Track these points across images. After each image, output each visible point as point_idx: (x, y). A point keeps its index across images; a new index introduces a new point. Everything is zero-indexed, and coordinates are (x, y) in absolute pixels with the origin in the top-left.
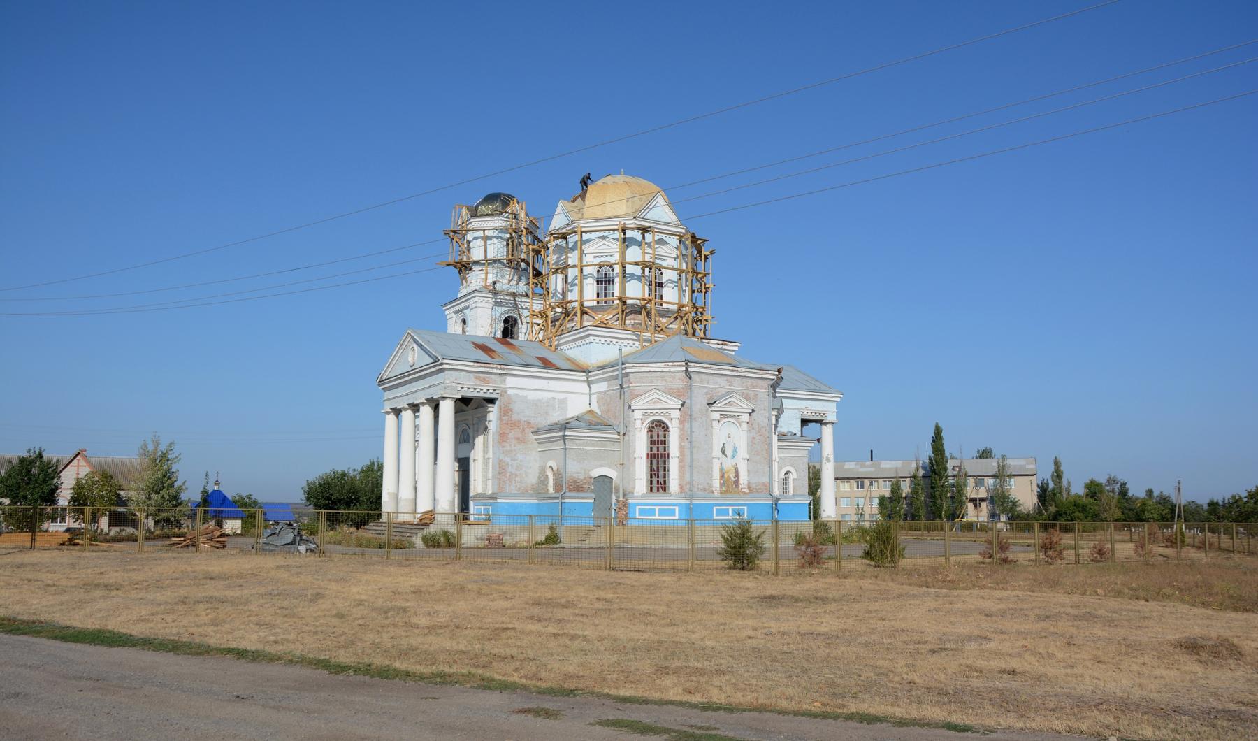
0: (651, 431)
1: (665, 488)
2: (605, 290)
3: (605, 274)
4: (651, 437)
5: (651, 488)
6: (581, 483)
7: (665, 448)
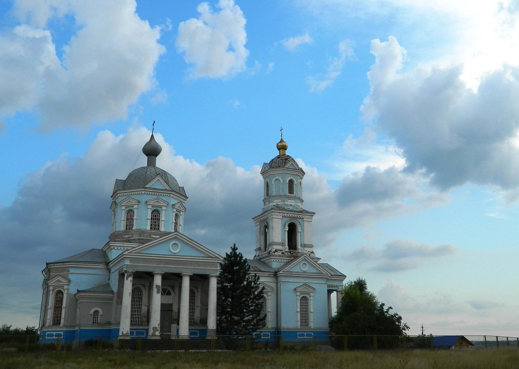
2: (155, 223)
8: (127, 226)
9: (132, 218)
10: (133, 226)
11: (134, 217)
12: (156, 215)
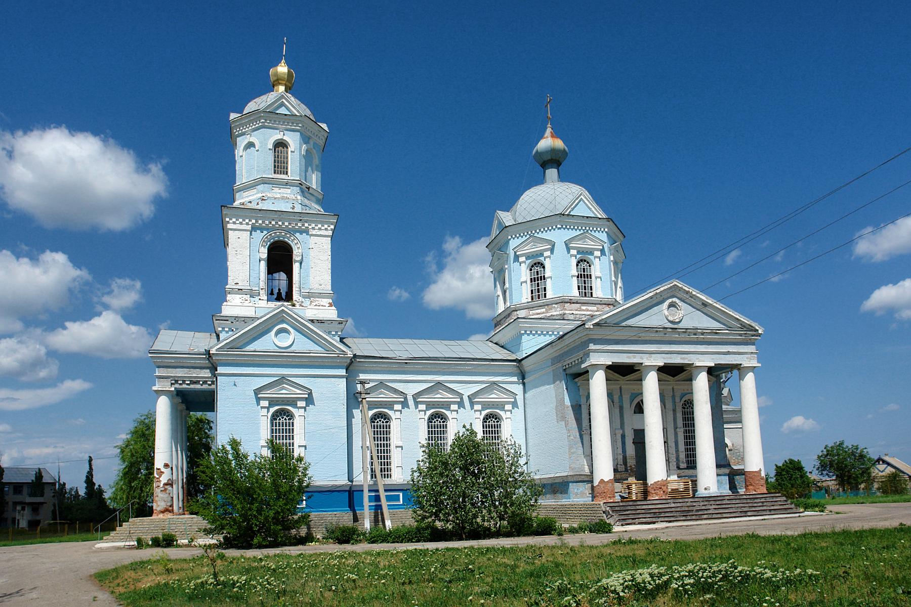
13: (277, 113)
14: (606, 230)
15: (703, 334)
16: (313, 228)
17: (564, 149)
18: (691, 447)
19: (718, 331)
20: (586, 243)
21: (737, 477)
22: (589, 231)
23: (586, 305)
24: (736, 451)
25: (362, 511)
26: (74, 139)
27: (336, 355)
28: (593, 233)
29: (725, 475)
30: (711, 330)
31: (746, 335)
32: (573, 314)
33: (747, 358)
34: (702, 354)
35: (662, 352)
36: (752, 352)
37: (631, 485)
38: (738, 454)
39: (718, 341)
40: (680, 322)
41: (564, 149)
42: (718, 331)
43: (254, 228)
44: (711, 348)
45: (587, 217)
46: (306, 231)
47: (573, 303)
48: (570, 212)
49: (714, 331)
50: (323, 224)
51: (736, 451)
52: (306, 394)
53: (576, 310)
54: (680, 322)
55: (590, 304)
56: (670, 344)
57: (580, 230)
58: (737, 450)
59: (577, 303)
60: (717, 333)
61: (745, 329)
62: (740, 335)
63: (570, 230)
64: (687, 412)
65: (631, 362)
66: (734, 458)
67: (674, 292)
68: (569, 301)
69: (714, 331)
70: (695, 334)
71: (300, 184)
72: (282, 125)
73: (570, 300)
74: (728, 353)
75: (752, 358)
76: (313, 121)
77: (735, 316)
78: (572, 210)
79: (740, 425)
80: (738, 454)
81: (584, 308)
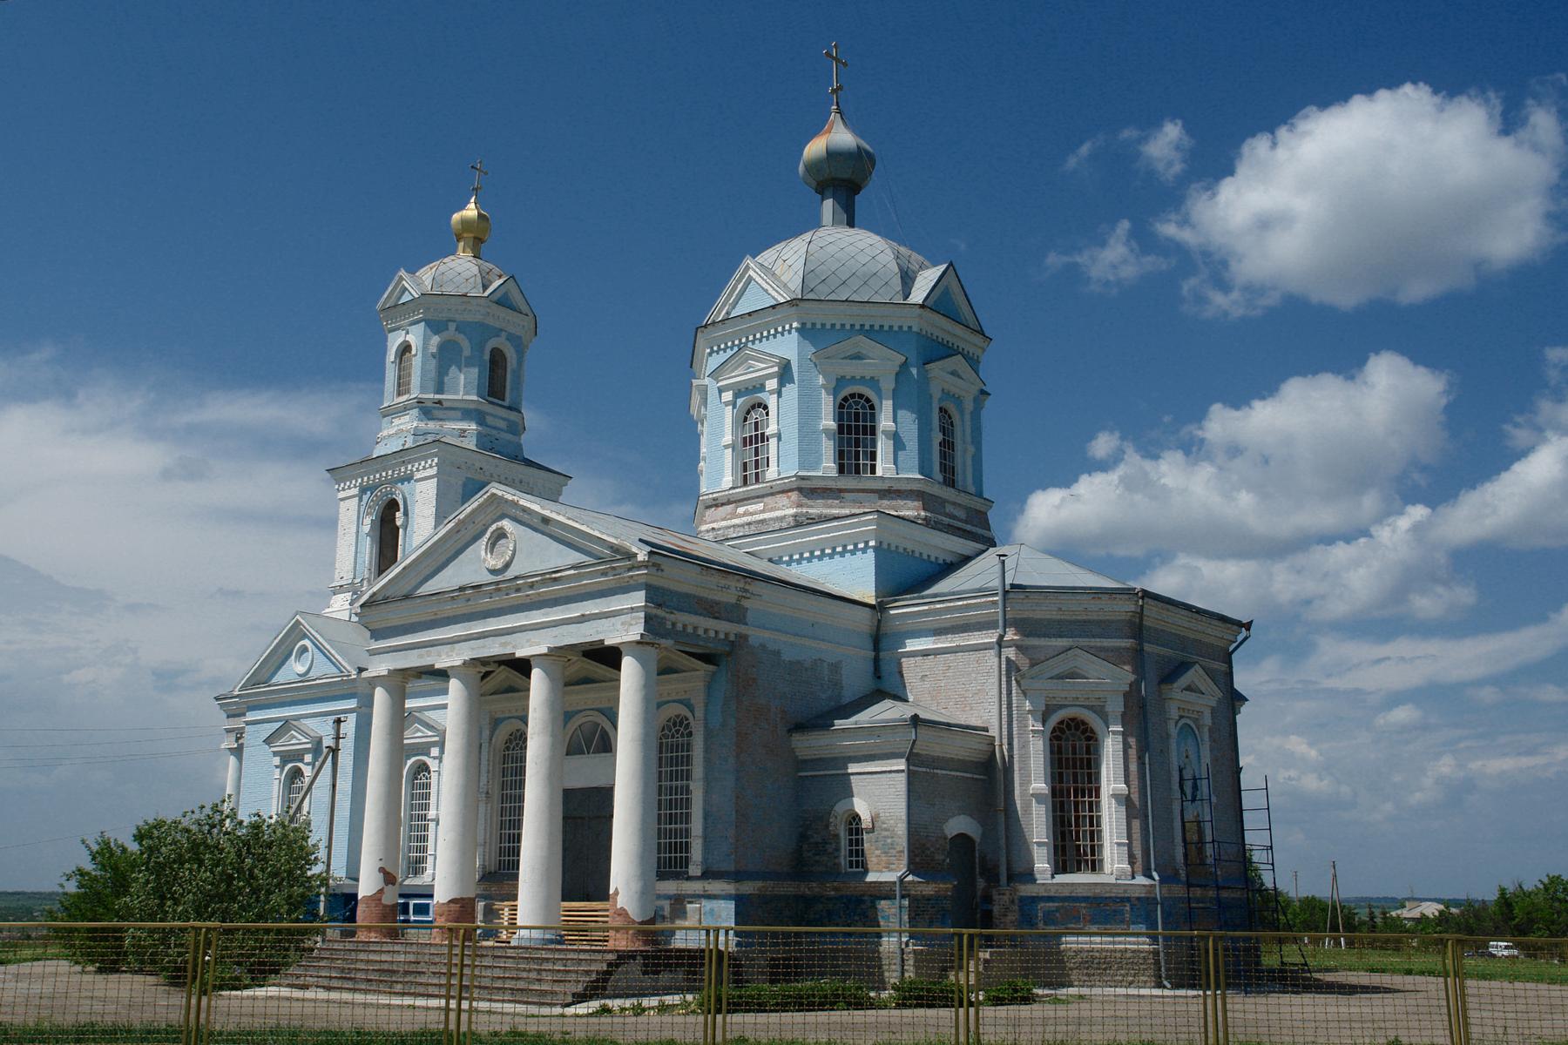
0: (1058, 738)
1: (1093, 862)
3: (857, 414)
4: (1060, 752)
5: (1064, 862)
6: (932, 849)
7: (1090, 775)
8: (745, 470)
9: (763, 434)
10: (768, 466)
11: (768, 426)
12: (857, 414)
13: (403, 304)
14: (795, 325)
15: (532, 586)
16: (418, 470)
17: (858, 147)
18: (422, 844)
19: (554, 576)
20: (752, 369)
21: (883, 902)
22: (750, 345)
23: (745, 502)
24: (886, 833)
25: (514, 921)
26: (1243, 170)
27: (339, 679)
28: (757, 346)
29: (727, 897)
30: (541, 575)
31: (617, 572)
32: (713, 529)
33: (622, 624)
34: (536, 630)
35: (470, 637)
36: (632, 608)
37: (503, 910)
38: (889, 841)
39: (569, 594)
40: (507, 566)
41: (858, 147)
42: (554, 576)
43: (363, 490)
44: (556, 613)
45: (749, 314)
46: (408, 478)
47: (723, 504)
48: (728, 313)
49: (548, 576)
50: (425, 458)
51: (886, 833)
52: (308, 743)
53: (723, 520)
54: (507, 566)
55: (753, 498)
56: (485, 618)
57: (732, 348)
58: (886, 830)
59: (729, 503)
60: (555, 579)
61: (619, 557)
62: (604, 573)
63: (786, 333)
64: (678, 746)
65: (424, 664)
66: (878, 852)
67: (502, 509)
68: (714, 503)
69: (548, 576)
70: (518, 590)
71: (418, 402)
72: (404, 320)
73: (714, 499)
74: (583, 619)
75: (633, 622)
76: (505, 281)
77: (591, 532)
78: (734, 308)
79: (898, 764)
80: (889, 841)
81: (741, 510)
